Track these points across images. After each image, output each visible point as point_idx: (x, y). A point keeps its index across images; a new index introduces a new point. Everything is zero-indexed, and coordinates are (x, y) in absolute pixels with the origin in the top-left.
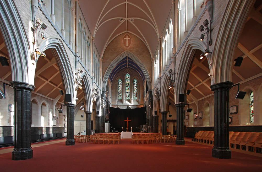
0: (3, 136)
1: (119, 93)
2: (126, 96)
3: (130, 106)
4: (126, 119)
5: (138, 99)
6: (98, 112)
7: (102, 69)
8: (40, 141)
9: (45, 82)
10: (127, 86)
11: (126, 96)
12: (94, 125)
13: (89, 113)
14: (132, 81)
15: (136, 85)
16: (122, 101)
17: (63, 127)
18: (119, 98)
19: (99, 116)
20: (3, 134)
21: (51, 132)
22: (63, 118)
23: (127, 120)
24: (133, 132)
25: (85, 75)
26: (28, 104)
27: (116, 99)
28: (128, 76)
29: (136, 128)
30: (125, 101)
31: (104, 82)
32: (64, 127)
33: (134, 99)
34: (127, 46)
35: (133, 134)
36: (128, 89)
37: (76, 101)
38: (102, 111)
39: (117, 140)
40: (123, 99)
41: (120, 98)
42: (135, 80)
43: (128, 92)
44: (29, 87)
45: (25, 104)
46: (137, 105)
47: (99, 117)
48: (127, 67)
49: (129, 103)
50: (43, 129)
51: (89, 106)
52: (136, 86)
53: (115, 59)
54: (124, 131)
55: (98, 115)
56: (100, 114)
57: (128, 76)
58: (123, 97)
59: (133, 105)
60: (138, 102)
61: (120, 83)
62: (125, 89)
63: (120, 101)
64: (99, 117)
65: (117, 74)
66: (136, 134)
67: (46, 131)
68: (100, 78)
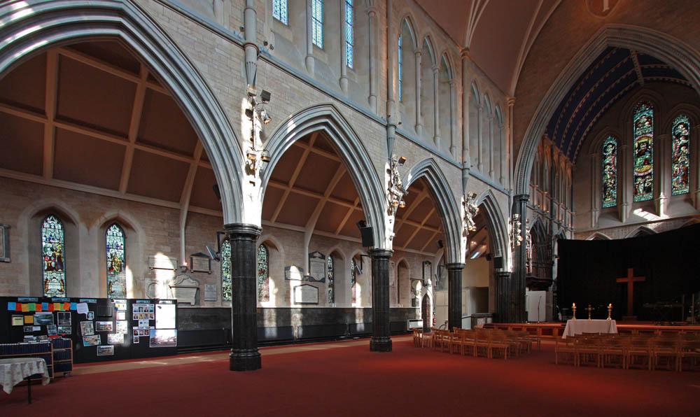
0: (277, 325)
1: (606, 187)
2: (636, 193)
3: (651, 227)
4: (625, 276)
5: (693, 193)
6: (500, 262)
7: (514, 128)
8: (348, 338)
9: (350, 208)
10: (641, 154)
11: (636, 193)
12: (502, 300)
13: (454, 267)
14: (663, 131)
15: (686, 138)
16: (616, 213)
17: (410, 307)
18: (605, 205)
19: (503, 273)
20: (277, 321)
21: (296, 321)
22: (410, 283)
23: (630, 279)
24: (618, 317)
25: (488, 197)
26: (247, 265)
27: (591, 211)
28: (644, 118)
29: (647, 305)
30: (634, 208)
31: (523, 166)
32: (413, 306)
33: (673, 196)
34: (606, 8)
35: (618, 328)
36: (647, 162)
37: (391, 242)
38: (514, 258)
39: (668, 351)
40: (622, 203)
41: (609, 202)
42: (677, 122)
43: (643, 177)
44: (246, 230)
45: (241, 264)
46: (690, 217)
47: (505, 275)
48: (638, 84)
49: (650, 217)
50: (357, 311)
51: (453, 248)
52: (683, 141)
53: (557, 80)
54: (577, 318)
55: (501, 270)
56: (509, 267)
57: (644, 118)
58: (620, 199)
59: (666, 217)
60: (692, 204)
61: (610, 150)
62: (633, 168)
63: (608, 213)
64: (502, 276)
65: (598, 119)
66: (633, 328)
67: (364, 317)
68: (507, 156)
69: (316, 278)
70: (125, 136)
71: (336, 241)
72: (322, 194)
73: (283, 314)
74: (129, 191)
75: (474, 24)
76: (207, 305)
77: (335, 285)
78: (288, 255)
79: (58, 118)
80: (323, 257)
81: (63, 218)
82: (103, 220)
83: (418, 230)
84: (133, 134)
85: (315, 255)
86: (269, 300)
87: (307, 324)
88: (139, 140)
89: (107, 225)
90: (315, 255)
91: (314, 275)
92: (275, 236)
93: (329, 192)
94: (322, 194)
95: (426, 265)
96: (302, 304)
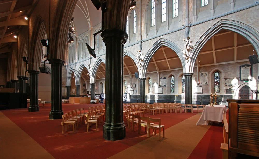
21: (156, 99)
69: (162, 85)
70: (165, 59)
71: (171, 71)
72: (234, 46)
74: (217, 62)
75: (88, 17)
76: (135, 94)
77: (171, 87)
78: (153, 80)
79: (168, 59)
80: (165, 78)
81: (174, 76)
82: (212, 71)
83: (85, 75)
84: (166, 58)
85: (162, 78)
86: (148, 94)
87: (159, 100)
89: (215, 72)
90: (162, 78)
91: (161, 84)
93: (236, 44)
94: (234, 46)
95: (241, 68)
96: (197, 93)
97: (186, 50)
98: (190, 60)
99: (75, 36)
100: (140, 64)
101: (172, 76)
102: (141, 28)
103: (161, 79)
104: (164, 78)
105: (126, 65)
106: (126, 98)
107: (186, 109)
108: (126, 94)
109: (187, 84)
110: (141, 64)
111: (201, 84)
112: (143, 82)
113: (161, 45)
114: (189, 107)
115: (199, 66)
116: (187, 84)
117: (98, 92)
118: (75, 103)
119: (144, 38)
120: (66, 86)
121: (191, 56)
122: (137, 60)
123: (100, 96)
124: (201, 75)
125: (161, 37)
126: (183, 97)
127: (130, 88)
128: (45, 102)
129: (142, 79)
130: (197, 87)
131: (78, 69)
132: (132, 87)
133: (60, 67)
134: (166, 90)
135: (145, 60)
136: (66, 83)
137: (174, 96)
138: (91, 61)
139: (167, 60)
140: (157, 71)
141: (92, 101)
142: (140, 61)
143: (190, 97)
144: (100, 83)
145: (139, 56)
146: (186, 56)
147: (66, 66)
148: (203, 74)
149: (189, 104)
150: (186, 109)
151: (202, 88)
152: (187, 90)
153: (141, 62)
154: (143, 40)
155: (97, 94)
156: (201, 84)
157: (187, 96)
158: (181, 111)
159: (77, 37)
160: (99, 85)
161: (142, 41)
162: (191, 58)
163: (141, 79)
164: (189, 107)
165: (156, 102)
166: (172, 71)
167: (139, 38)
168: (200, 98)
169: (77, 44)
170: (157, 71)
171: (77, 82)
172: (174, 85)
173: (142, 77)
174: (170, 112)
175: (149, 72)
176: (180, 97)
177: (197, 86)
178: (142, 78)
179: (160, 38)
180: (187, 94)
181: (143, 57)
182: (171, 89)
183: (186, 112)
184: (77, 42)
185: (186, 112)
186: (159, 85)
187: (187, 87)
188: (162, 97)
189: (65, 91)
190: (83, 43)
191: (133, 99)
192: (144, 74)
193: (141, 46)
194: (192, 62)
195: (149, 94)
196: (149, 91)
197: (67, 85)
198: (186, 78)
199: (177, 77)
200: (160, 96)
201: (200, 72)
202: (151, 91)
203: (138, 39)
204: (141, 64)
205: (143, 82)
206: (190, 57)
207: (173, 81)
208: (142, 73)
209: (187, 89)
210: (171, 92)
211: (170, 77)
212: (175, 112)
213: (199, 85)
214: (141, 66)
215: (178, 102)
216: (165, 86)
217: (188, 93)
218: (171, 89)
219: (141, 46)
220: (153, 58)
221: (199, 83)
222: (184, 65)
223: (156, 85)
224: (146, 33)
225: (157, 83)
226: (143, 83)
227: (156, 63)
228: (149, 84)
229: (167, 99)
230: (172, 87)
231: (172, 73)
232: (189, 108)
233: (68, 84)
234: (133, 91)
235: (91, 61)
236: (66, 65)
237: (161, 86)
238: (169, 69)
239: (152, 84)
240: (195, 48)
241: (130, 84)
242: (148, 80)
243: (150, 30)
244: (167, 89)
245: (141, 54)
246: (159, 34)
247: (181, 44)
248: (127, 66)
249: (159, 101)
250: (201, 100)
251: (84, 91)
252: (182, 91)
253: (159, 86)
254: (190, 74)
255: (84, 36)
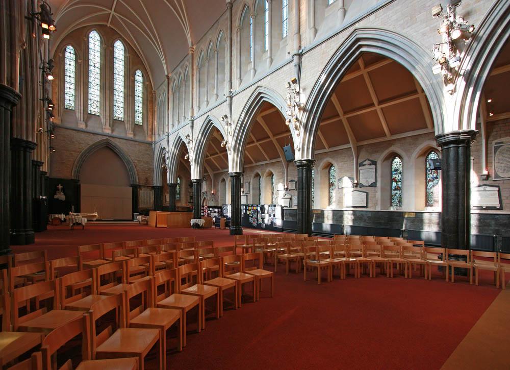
21: (348, 221)
28: (95, 40)
69: (365, 184)
70: (372, 105)
71: (390, 143)
73: (338, 215)
78: (340, 169)
79: (380, 103)
80: (374, 163)
81: (400, 157)
84: (375, 101)
87: (356, 225)
88: (380, 102)
91: (362, 181)
92: (331, 158)
96: (353, 207)
97: (446, 48)
98: (464, 83)
99: (166, 74)
100: (294, 117)
101: (393, 155)
102: (299, 16)
103: (362, 165)
104: (370, 162)
105: (272, 133)
106: (274, 216)
107: (450, 267)
108: (273, 208)
109: (452, 173)
110: (297, 119)
111: (497, 176)
112: (304, 173)
113: (357, 53)
114: (457, 257)
115: (489, 120)
116: (452, 173)
117: (217, 201)
118: (158, 226)
119: (308, 40)
120: (153, 188)
121: (467, 66)
122: (288, 109)
123: (220, 210)
124: (496, 149)
125: (357, 26)
126: (430, 220)
127: (282, 193)
128: (88, 221)
129: (304, 163)
130: (482, 188)
131: (171, 149)
132: (287, 189)
133: (9, 112)
134: (375, 196)
135: (309, 107)
136: (153, 180)
137: (401, 215)
138: (192, 127)
139: (378, 108)
140: (351, 145)
141: (193, 221)
142: (297, 108)
143: (461, 222)
144: (220, 181)
145: (293, 96)
146: (444, 72)
147: (153, 143)
148: (502, 143)
149: (458, 248)
150: (450, 267)
151: (499, 191)
152: (452, 197)
153: (299, 113)
154: (303, 48)
155: (216, 205)
156: (497, 176)
157: (452, 217)
158: (428, 272)
159: (170, 75)
160: (218, 185)
161: (300, 51)
162: (468, 77)
163: (299, 163)
164: (457, 257)
165: (347, 230)
166: (394, 140)
167: (293, 45)
168: (489, 225)
169: (170, 92)
170: (351, 145)
171: (170, 179)
172: (400, 183)
173: (302, 157)
174: (385, 274)
175: (330, 147)
176: (418, 218)
177: (479, 186)
178: (301, 161)
179: (351, 29)
180: (450, 210)
181: (303, 99)
182: (391, 196)
183: (450, 279)
184: (170, 86)
185: (450, 279)
186: (357, 184)
187: (452, 182)
188: (366, 218)
189: (150, 198)
190: (180, 87)
191: (290, 219)
192: (308, 148)
193: (299, 67)
194: (471, 89)
195: (328, 208)
196: (329, 200)
197: (155, 185)
198: (446, 153)
199: (409, 157)
200: (358, 214)
201: (491, 138)
202: (334, 199)
203: (292, 47)
204: (297, 119)
205: (304, 173)
206: (462, 73)
207: (397, 170)
208: (303, 144)
209: (452, 191)
210: (391, 203)
211: (390, 161)
212: (403, 275)
213: (488, 182)
214: (298, 124)
215: (414, 235)
216: (374, 185)
217: (457, 205)
218: (391, 196)
219: (299, 67)
220: (334, 99)
221: (488, 176)
222: (437, 107)
223: (347, 183)
224: (312, 25)
225: (351, 178)
226: (304, 175)
227: (348, 119)
228: (331, 181)
229: (380, 224)
230: (393, 188)
231: (394, 148)
232: (461, 264)
233: (157, 182)
234: (291, 199)
235: (192, 127)
236: (153, 140)
237: (362, 186)
238: (385, 135)
239: (336, 180)
240: (484, 34)
241: (283, 182)
242: (327, 170)
243: (326, 15)
244: (379, 195)
245: (298, 90)
246: (349, 19)
247: (424, 34)
248: (274, 135)
249: (355, 230)
250: (497, 232)
251: (190, 200)
252: (427, 202)
253: (357, 185)
254: (462, 137)
255: (181, 71)
